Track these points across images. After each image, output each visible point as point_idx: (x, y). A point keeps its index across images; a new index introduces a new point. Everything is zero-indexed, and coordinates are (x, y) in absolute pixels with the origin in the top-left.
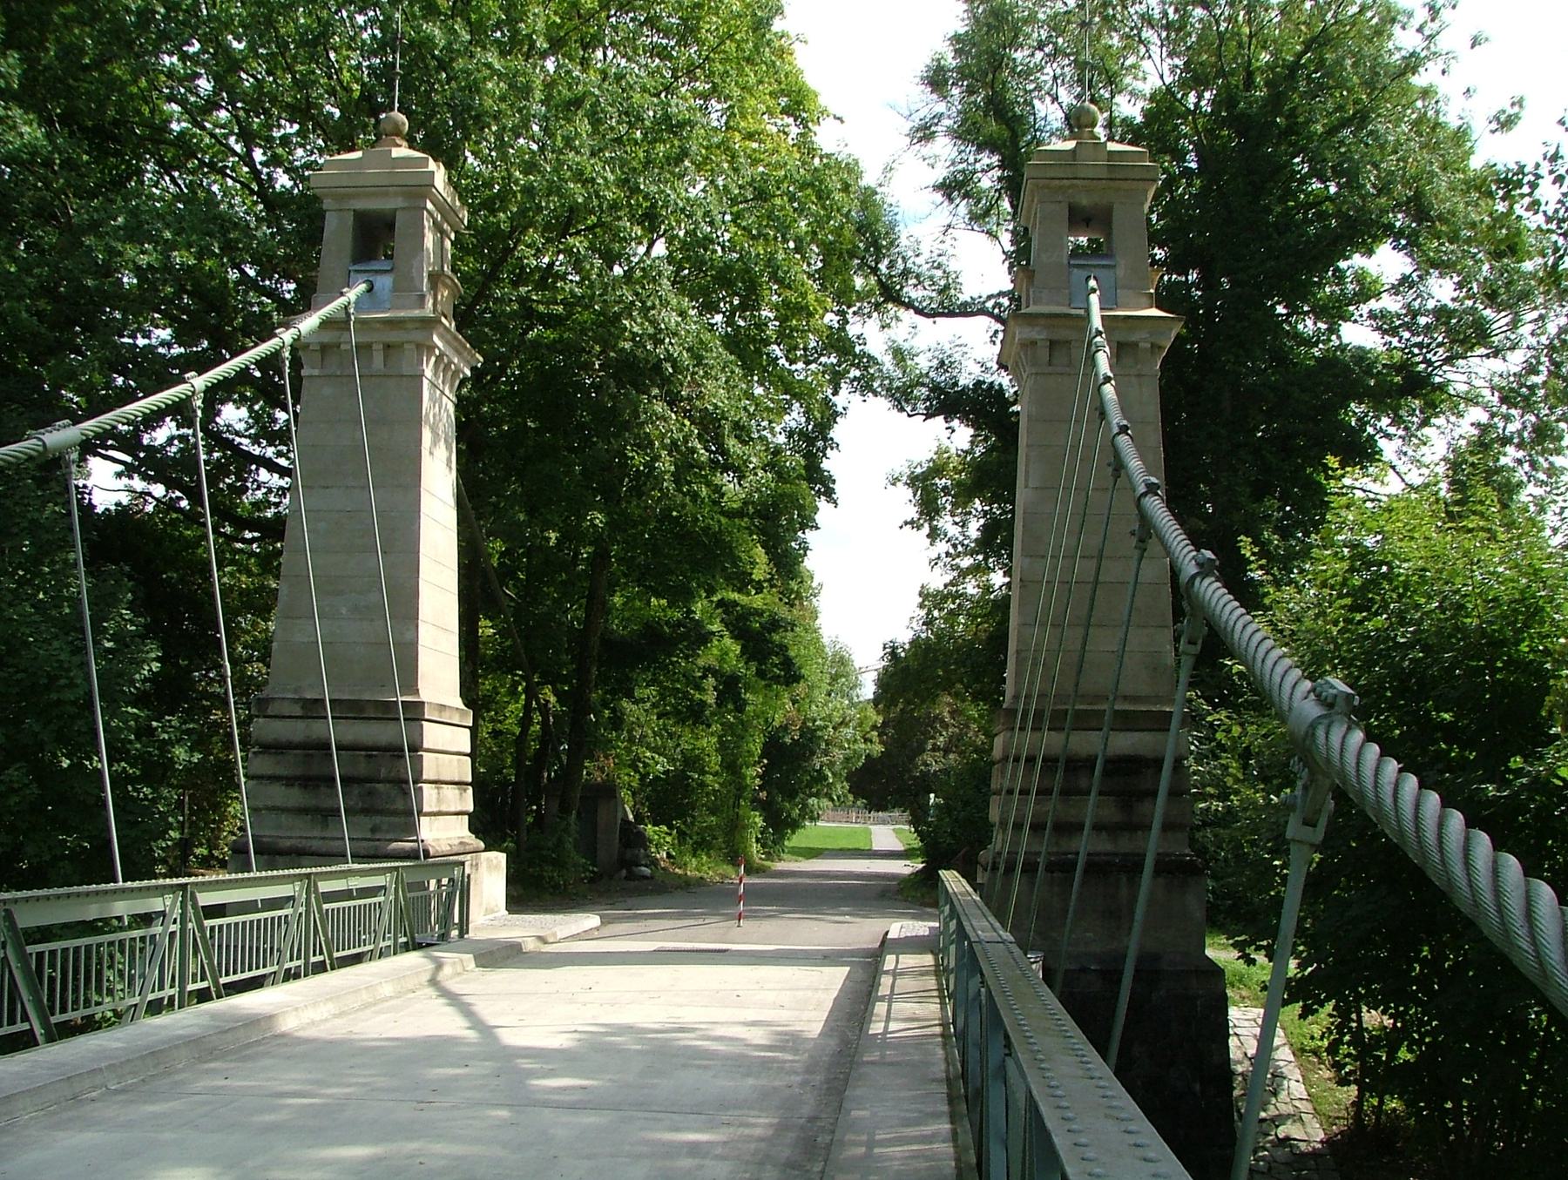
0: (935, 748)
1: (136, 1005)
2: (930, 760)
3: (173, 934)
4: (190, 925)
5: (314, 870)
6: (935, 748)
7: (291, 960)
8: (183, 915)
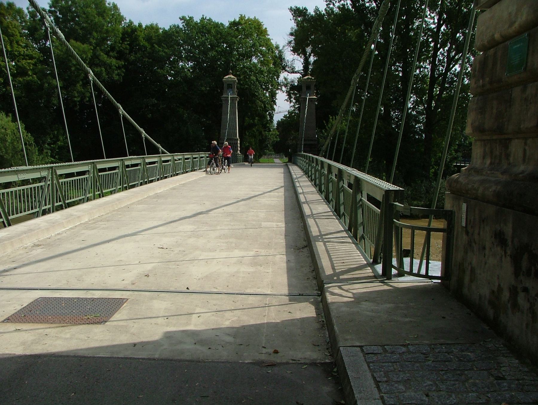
3: (49, 185)
4: (55, 182)
5: (124, 158)
7: (46, 205)
8: (52, 178)
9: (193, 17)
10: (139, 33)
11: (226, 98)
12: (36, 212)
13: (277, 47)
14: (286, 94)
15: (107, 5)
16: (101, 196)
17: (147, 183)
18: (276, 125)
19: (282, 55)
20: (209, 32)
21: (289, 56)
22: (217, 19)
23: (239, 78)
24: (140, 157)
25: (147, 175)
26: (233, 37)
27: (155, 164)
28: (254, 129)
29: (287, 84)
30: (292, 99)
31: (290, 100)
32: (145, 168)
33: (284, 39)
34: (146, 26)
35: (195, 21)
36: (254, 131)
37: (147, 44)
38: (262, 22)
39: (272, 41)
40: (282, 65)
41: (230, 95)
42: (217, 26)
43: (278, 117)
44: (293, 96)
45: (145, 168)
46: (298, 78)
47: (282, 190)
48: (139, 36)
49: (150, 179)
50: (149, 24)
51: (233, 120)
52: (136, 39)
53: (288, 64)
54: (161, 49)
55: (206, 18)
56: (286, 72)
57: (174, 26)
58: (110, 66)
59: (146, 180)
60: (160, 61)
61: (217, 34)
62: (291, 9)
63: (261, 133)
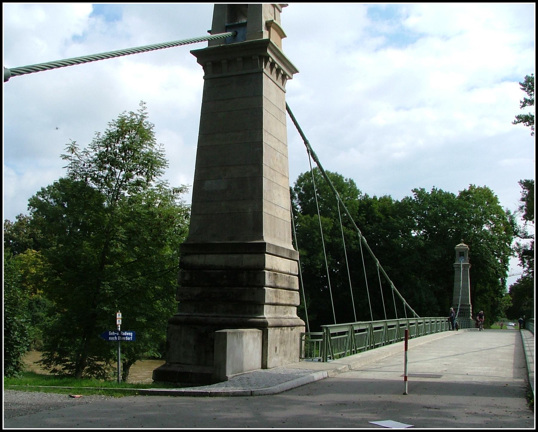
0: (525, 305)
1: (344, 354)
2: (523, 308)
6: (525, 305)
9: (424, 189)
10: (374, 205)
11: (457, 266)
12: (363, 349)
13: (508, 213)
14: (519, 259)
15: (345, 181)
16: (355, 353)
17: (373, 348)
18: (509, 290)
19: (513, 220)
20: (440, 202)
21: (519, 221)
22: (446, 189)
23: (470, 245)
24: (347, 325)
25: (374, 341)
26: (463, 206)
27: (381, 329)
28: (485, 295)
29: (520, 249)
30: (525, 264)
31: (523, 264)
32: (353, 337)
33: (515, 204)
34: (380, 198)
35: (426, 192)
36: (485, 297)
37: (382, 216)
38: (492, 191)
39: (502, 208)
40: (513, 230)
41: (463, 263)
42: (449, 196)
43: (511, 281)
44: (527, 261)
45: (353, 337)
46: (531, 242)
47: (514, 346)
48: (374, 208)
49: (375, 344)
50: (382, 195)
51: (465, 287)
52: (372, 211)
53: (519, 230)
54: (396, 220)
55: (437, 189)
56: (518, 237)
57: (407, 198)
58: (348, 236)
59: (372, 345)
60: (394, 231)
61: (449, 205)
62: (521, 182)
63: (493, 299)
